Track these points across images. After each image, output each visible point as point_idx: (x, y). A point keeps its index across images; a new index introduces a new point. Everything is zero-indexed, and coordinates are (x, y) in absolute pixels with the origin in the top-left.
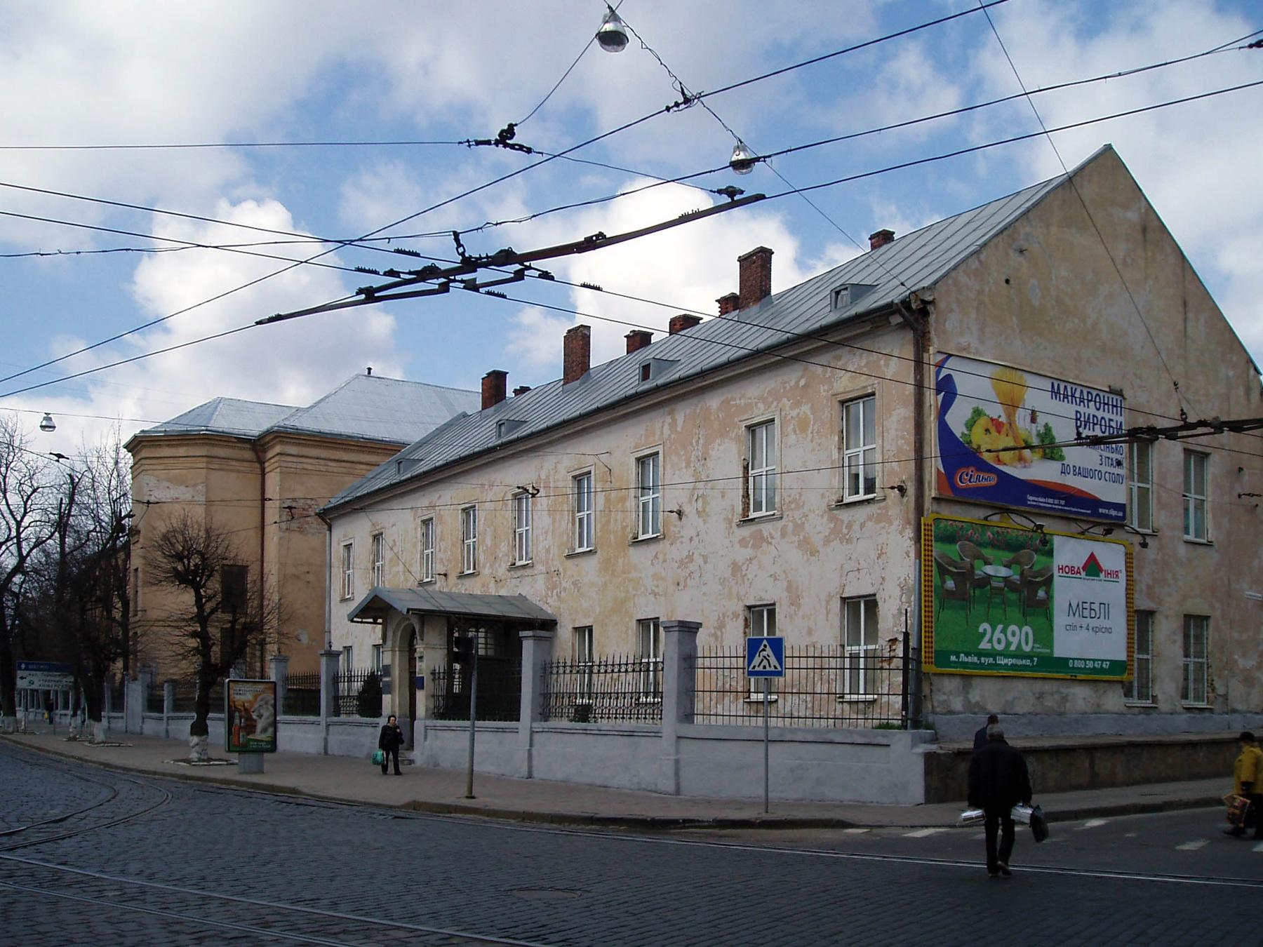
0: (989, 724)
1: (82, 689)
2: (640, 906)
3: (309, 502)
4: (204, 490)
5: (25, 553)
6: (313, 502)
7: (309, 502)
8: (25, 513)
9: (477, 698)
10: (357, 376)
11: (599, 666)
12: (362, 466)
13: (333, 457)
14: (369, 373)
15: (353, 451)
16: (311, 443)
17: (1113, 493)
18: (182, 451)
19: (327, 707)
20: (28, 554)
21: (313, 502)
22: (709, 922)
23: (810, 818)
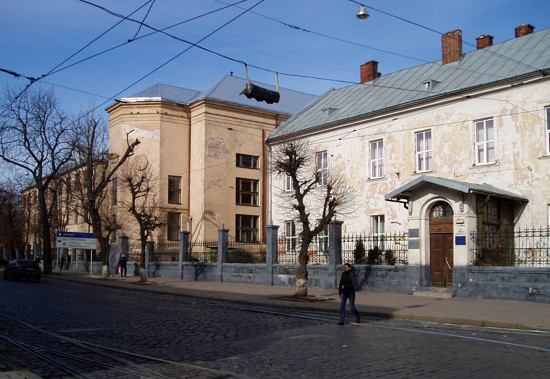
0: (156, 270)
1: (26, 249)
2: (369, 354)
3: (220, 140)
4: (160, 133)
5: (56, 166)
6: (222, 141)
7: (220, 140)
8: (57, 144)
9: (92, 259)
10: (227, 75)
11: (201, 243)
12: (246, 122)
13: (231, 116)
14: (232, 75)
15: (241, 113)
16: (218, 107)
17: (78, 221)
18: (146, 110)
19: (223, 253)
20: (58, 168)
21: (222, 141)
22: (406, 362)
23: (381, 306)
